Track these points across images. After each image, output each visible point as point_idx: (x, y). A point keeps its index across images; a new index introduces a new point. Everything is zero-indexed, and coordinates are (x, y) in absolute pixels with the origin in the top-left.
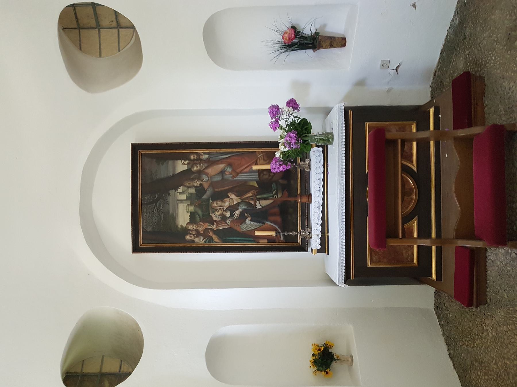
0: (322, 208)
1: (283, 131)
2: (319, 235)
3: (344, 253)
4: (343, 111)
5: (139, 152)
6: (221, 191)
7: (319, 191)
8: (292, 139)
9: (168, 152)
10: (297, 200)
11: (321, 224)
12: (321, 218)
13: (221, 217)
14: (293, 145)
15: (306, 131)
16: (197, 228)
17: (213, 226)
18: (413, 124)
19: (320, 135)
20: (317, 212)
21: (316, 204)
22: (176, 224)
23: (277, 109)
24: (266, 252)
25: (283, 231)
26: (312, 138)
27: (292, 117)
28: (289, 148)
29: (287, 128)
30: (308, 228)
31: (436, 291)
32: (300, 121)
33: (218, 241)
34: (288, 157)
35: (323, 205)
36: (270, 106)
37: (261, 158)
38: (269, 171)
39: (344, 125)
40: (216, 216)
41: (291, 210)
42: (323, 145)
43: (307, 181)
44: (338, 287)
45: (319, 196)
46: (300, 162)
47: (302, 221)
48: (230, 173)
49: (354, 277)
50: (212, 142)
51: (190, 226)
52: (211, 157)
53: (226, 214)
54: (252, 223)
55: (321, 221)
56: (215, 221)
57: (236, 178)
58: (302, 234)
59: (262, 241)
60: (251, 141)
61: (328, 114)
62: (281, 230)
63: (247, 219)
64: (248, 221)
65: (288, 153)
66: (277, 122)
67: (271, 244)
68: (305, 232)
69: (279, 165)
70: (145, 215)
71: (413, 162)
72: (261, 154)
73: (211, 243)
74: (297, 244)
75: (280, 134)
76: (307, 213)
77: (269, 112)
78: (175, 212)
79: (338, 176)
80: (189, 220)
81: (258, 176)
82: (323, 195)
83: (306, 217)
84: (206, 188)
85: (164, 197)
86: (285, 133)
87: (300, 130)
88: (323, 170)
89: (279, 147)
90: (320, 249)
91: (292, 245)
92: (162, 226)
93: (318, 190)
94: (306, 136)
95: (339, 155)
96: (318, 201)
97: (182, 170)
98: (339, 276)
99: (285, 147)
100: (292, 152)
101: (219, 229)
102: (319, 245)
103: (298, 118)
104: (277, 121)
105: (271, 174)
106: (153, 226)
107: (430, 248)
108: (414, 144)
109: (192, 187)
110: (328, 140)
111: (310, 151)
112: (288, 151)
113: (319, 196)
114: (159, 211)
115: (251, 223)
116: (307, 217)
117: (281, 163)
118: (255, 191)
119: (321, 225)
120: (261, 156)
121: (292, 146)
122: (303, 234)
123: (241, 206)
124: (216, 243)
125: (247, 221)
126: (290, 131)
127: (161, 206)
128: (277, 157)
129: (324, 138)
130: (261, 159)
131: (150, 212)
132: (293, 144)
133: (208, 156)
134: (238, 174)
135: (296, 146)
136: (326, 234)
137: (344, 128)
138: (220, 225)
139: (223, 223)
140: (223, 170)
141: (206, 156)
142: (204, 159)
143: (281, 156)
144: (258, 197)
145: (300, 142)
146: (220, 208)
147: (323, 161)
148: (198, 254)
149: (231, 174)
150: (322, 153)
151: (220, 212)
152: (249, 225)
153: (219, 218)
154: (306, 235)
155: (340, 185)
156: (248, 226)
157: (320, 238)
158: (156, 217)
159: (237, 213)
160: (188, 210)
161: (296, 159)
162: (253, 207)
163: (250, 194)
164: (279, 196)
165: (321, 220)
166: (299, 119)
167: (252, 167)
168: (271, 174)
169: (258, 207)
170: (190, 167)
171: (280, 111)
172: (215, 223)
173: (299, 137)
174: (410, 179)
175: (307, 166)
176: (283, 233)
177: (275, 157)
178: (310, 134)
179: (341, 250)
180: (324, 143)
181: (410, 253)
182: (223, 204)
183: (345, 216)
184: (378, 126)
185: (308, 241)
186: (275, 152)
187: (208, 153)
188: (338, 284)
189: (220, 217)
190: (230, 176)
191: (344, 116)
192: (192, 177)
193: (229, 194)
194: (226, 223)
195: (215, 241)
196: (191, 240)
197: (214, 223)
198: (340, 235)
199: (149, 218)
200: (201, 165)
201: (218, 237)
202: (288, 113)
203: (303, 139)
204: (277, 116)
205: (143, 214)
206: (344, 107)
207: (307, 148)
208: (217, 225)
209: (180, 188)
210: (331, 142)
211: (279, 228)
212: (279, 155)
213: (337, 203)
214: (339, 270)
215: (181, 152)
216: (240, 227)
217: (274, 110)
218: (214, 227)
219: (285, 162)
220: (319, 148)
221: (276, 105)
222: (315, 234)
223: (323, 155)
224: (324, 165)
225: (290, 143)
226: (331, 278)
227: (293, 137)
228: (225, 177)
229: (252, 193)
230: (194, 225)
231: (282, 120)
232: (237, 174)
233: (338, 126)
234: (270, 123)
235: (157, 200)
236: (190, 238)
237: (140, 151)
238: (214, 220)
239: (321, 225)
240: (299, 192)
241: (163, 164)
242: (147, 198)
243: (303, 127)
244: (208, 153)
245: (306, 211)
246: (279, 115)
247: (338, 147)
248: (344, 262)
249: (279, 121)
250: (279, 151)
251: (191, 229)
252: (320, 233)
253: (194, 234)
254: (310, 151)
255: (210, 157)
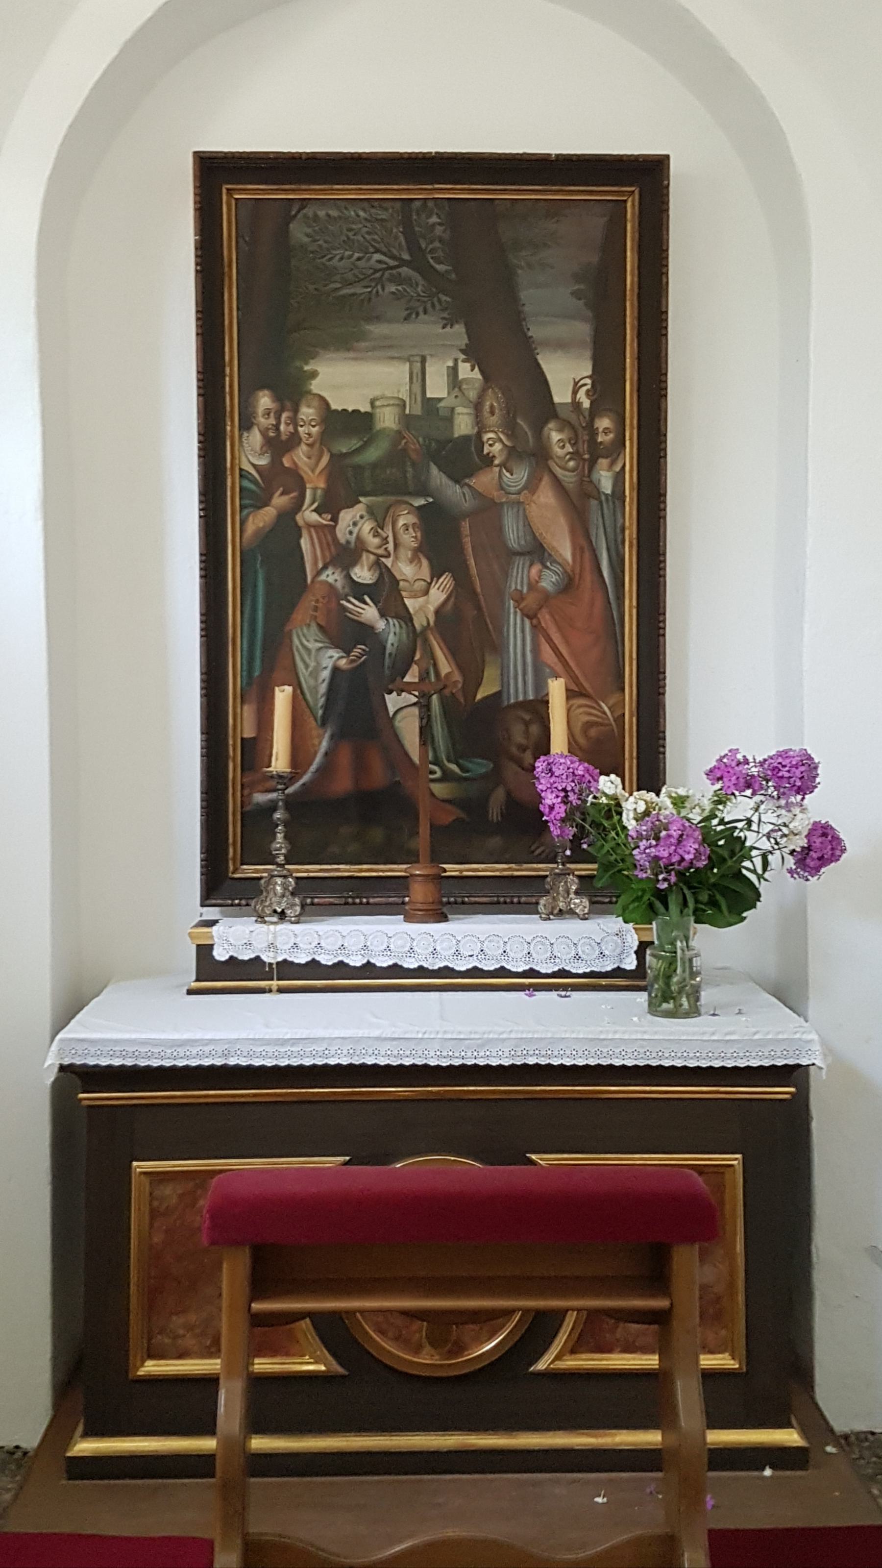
0: (385, 965)
1: (708, 806)
2: (271, 954)
3: (194, 1063)
4: (791, 1062)
5: (633, 192)
6: (462, 550)
7: (457, 953)
8: (673, 848)
9: (628, 320)
10: (417, 862)
11: (318, 963)
12: (341, 963)
13: (353, 545)
14: (647, 851)
15: (705, 904)
16: (304, 439)
17: (315, 510)
18: (733, 1359)
19: (691, 960)
20: (368, 944)
21: (400, 942)
22: (322, 352)
23: (798, 783)
24: (202, 733)
25: (290, 804)
26: (677, 927)
27: (765, 844)
28: (634, 834)
29: (719, 824)
30: (303, 906)
31: (25, 1453)
32: (749, 880)
33: (251, 527)
34: (596, 825)
35: (396, 970)
36: (813, 756)
37: (599, 714)
38: (543, 747)
39: (730, 1064)
40: (355, 524)
41: (377, 835)
42: (645, 973)
43: (498, 903)
44: (48, 1039)
45: (434, 952)
46: (576, 873)
47: (340, 881)
48: (537, 582)
49: (90, 1107)
50: (665, 510)
51: (311, 411)
52: (605, 505)
53: (362, 566)
54: (326, 674)
55: (330, 963)
56: (335, 519)
57: (512, 610)
58: (279, 881)
59: (248, 713)
60: (667, 674)
61: (774, 996)
62: (295, 793)
63: (344, 655)
64: (332, 658)
65: (614, 829)
66: (746, 782)
67: (234, 749)
68: (283, 896)
69: (564, 790)
70: (361, 213)
71: (573, 1356)
72: (612, 713)
73: (240, 499)
74: (234, 859)
75: (694, 795)
76: (365, 900)
77: (786, 752)
78: (374, 349)
79: (519, 1036)
80: (340, 409)
81: (522, 703)
82: (440, 969)
83: (350, 897)
84: (473, 482)
85: (439, 301)
86: (700, 815)
87: (712, 880)
88: (543, 971)
89: (638, 790)
90: (213, 957)
91: (231, 840)
92: (311, 287)
93: (462, 951)
94: (685, 904)
95: (605, 1042)
96: (415, 949)
97: (549, 377)
98: (93, 1042)
99: (640, 818)
100: (618, 844)
101: (300, 536)
102: (231, 954)
103: (760, 871)
104: (749, 783)
105: (528, 757)
106: (310, 249)
107: (208, 1428)
108: (651, 1361)
109: (478, 423)
110: (666, 996)
111: (621, 919)
112: (624, 828)
113: (434, 952)
114: (378, 275)
115: (325, 668)
116: (346, 904)
117: (572, 797)
118: (460, 686)
119: (313, 960)
120: (604, 713)
121: (642, 848)
122: (278, 888)
123: (398, 630)
124: (243, 523)
125: (335, 653)
126: (708, 837)
127: (400, 288)
128: (597, 781)
129: (675, 979)
130: (590, 714)
131: (376, 237)
132: (653, 850)
133: (609, 492)
134: (530, 618)
135: (642, 862)
136: (275, 984)
137: (717, 1064)
138: (316, 541)
139: (327, 554)
140: (550, 555)
141: (606, 485)
142: (595, 476)
143: (604, 800)
144: (435, 697)
145: (661, 877)
146: (391, 539)
147: (580, 971)
148: (195, 445)
149: (532, 587)
150: (615, 966)
151: (373, 542)
152: (318, 663)
153: (348, 536)
154: (273, 899)
155: (479, 1046)
156: (313, 659)
157: (258, 958)
158: (353, 264)
159: (369, 613)
160: (383, 406)
161: (588, 858)
162: (393, 681)
163: (445, 666)
164: (437, 788)
165: (336, 961)
166: (759, 877)
167: (557, 677)
168: (528, 757)
169: (393, 701)
170: (563, 413)
171: (792, 799)
172: (324, 520)
173: (680, 874)
174: (500, 1342)
175: (561, 905)
176: (280, 803)
177: (601, 774)
178: (692, 919)
179: (207, 1049)
180: (656, 978)
181: (189, 1342)
182: (406, 554)
183: (351, 1066)
184: (728, 1207)
185: (247, 905)
186: (617, 775)
187: (618, 495)
188: (61, 1040)
189: (353, 539)
190: (522, 586)
191: (766, 1063)
192: (519, 421)
193: (446, 580)
194: (325, 567)
195: (251, 518)
196: (253, 415)
197: (324, 516)
198: (268, 1044)
199: (350, 230)
200: (572, 464)
201: (268, 529)
202: (780, 830)
203: (672, 891)
204: (770, 784)
205: (366, 205)
206: (808, 1065)
207: (638, 907)
208: (317, 527)
209: (477, 369)
210: (660, 1005)
211: (304, 784)
212: (607, 791)
213: (406, 1033)
214: (117, 1042)
215: (628, 376)
216: (309, 626)
217: (798, 773)
218: (309, 515)
219: (578, 814)
220: (634, 956)
221: (818, 780)
222: (275, 937)
223: (607, 972)
224: (563, 973)
225: (657, 838)
226: (87, 1004)
227: (680, 851)
228: (520, 563)
229: (449, 673)
230: (317, 428)
231: (752, 803)
232: (530, 615)
233: (728, 1038)
234: (740, 757)
235: (425, 271)
236: (260, 410)
237: (637, 192)
238: (338, 513)
239: (313, 960)
240: (452, 869)
241: (576, 294)
242: (434, 225)
243: (725, 891)
244: (618, 495)
245: (372, 900)
246: (775, 793)
247: (639, 1036)
248: (155, 1063)
249: (748, 792)
250: (624, 789)
251: (301, 416)
252: (280, 959)
253: (277, 427)
254: (621, 919)
255: (603, 498)
